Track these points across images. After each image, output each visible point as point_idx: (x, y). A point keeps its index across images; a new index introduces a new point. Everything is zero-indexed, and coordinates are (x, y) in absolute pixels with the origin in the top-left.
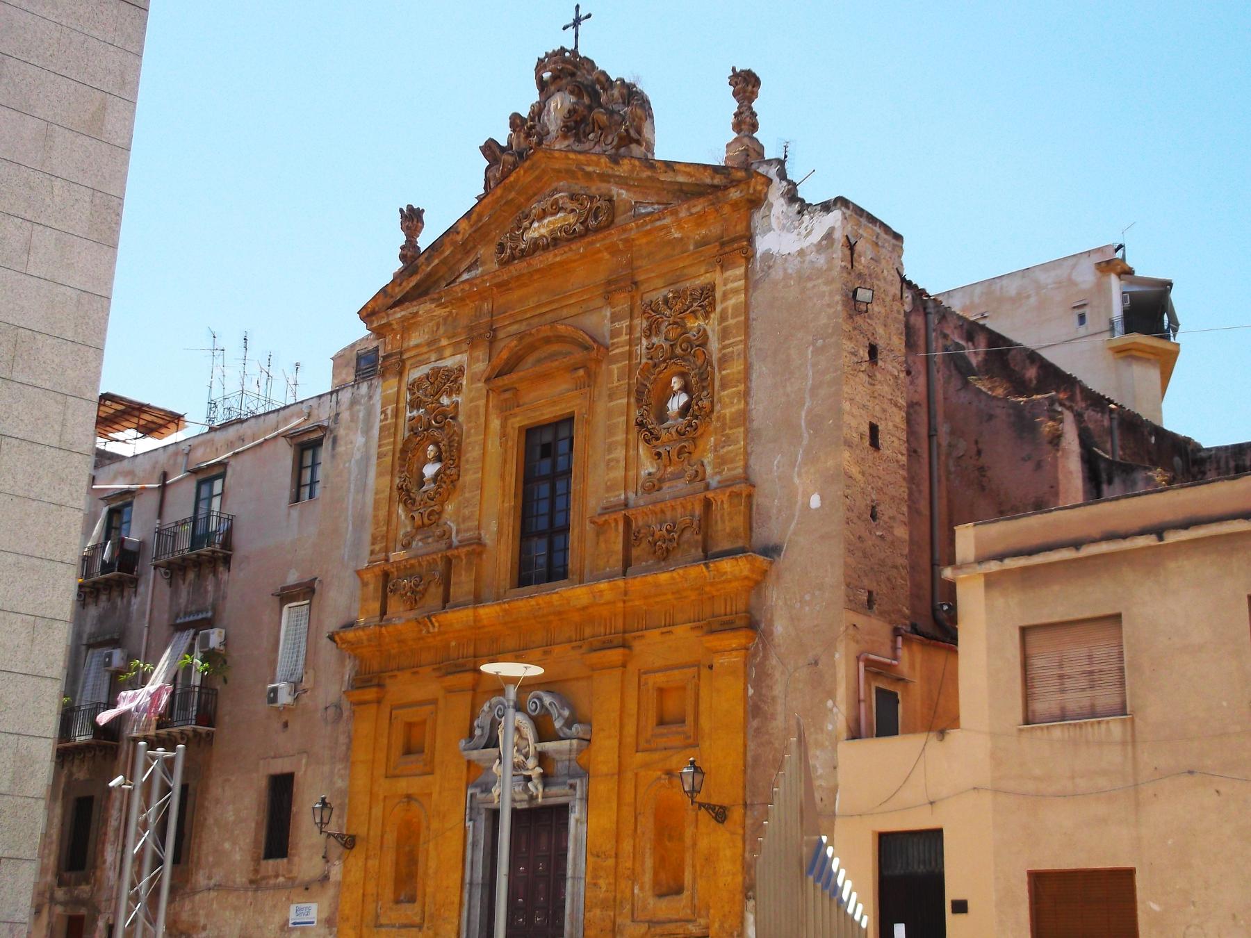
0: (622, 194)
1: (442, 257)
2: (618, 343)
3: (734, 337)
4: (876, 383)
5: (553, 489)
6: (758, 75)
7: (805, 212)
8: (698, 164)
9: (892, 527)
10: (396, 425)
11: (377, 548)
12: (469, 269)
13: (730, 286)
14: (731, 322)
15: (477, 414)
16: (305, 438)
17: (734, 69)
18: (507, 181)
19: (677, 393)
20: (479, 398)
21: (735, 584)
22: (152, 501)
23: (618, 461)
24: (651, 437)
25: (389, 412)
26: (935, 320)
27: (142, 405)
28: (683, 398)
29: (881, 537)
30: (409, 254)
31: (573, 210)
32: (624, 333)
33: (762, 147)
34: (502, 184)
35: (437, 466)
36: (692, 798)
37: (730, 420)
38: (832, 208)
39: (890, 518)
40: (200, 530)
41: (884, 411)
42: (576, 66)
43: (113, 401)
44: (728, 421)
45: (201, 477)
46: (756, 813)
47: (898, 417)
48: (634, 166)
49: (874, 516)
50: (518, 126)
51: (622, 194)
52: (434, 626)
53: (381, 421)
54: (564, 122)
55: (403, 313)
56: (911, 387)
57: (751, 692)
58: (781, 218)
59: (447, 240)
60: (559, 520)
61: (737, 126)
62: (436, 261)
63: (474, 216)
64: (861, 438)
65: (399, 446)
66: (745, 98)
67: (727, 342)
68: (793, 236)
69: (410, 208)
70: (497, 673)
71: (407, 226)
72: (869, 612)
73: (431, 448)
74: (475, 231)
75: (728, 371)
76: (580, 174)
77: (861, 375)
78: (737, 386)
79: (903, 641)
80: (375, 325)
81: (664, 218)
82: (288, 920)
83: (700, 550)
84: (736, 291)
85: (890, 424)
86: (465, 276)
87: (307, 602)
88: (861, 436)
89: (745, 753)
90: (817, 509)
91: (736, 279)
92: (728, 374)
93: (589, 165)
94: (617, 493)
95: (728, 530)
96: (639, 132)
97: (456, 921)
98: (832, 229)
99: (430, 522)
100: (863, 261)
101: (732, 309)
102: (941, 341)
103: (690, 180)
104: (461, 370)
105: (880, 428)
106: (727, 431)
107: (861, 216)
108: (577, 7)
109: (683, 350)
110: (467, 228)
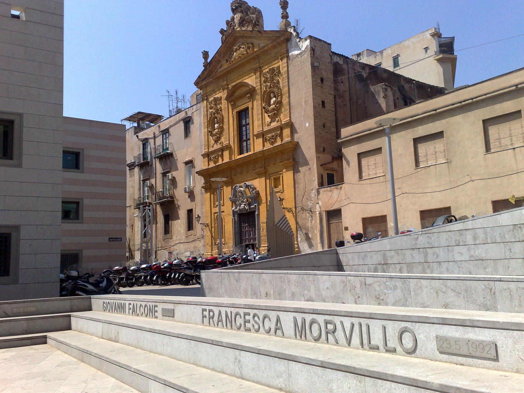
5: (246, 128)
8: (274, 31)
11: (206, 148)
12: (220, 68)
13: (283, 65)
20: (226, 105)
25: (205, 111)
26: (350, 66)
27: (149, 114)
28: (274, 99)
30: (206, 65)
31: (243, 48)
32: (259, 82)
33: (290, 22)
39: (329, 126)
40: (165, 148)
41: (326, 96)
42: (241, 4)
45: (163, 133)
47: (331, 98)
49: (324, 126)
61: (283, 18)
63: (219, 53)
69: (204, 51)
72: (324, 153)
77: (318, 87)
80: (199, 86)
84: (285, 67)
86: (220, 70)
88: (319, 104)
90: (308, 127)
96: (258, 22)
100: (318, 53)
102: (353, 71)
104: (221, 97)
107: (316, 40)
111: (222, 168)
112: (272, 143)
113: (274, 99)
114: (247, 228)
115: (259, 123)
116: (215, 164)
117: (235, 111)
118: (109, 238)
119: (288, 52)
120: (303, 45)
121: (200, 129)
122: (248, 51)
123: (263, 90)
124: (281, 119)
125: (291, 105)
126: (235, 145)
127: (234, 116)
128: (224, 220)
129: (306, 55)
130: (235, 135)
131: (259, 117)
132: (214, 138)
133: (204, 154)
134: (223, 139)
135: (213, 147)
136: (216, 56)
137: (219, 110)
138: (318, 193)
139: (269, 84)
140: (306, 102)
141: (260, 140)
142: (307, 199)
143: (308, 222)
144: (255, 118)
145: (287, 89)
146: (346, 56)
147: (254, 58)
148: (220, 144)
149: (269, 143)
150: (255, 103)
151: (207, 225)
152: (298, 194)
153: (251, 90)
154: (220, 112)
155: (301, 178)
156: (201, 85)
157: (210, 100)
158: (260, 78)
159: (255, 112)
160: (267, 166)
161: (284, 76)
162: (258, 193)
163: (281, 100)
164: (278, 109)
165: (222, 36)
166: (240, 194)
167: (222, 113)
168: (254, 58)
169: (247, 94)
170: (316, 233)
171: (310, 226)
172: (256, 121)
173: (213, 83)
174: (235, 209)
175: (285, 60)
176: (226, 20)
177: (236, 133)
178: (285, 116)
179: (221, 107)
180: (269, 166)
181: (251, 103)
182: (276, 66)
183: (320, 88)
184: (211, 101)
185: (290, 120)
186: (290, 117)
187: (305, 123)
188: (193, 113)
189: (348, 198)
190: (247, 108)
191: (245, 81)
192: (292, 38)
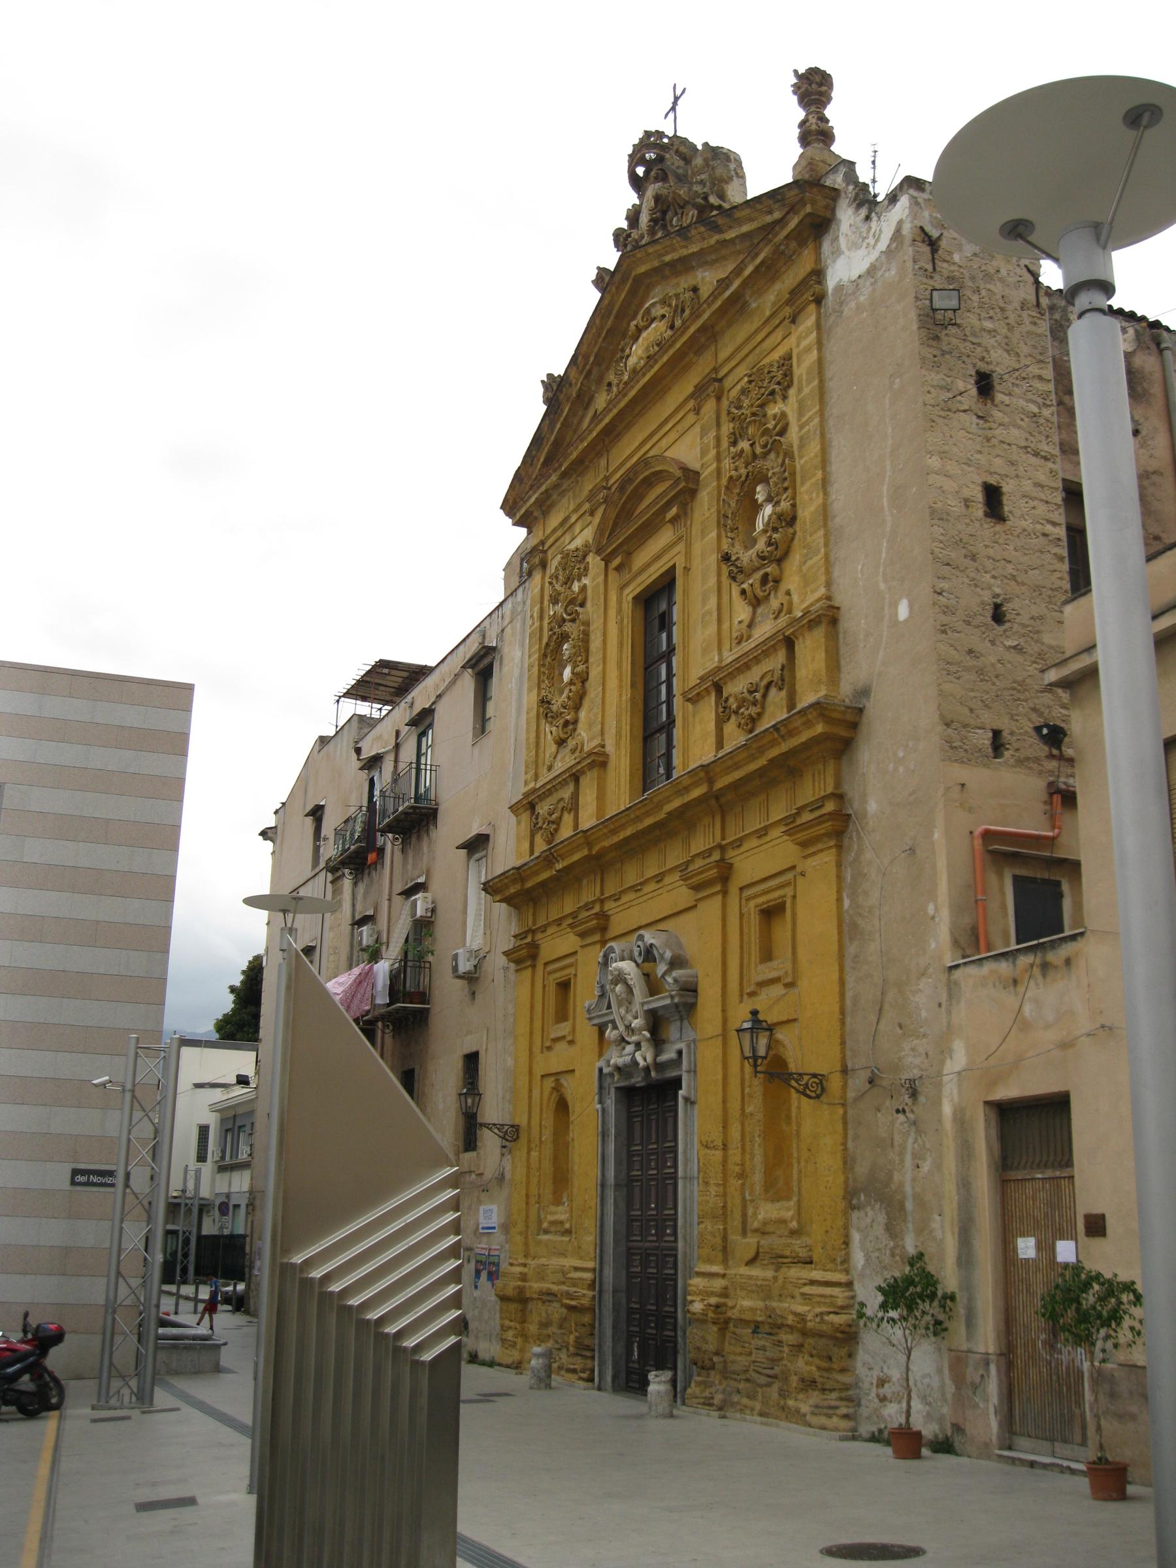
4: (994, 426)
6: (822, 68)
14: (806, 391)
17: (796, 72)
22: (391, 757)
23: (711, 613)
28: (768, 510)
31: (663, 316)
37: (811, 523)
43: (390, 668)
46: (857, 1081)
49: (998, 616)
53: (531, 626)
56: (1142, 451)
57: (846, 903)
61: (805, 138)
62: (558, 426)
64: (967, 506)
68: (862, 252)
84: (808, 350)
88: (967, 503)
89: (842, 995)
98: (900, 223)
105: (1004, 490)
114: (637, 1166)
118: (75, 1172)
120: (884, 229)
138: (952, 989)
143: (902, 1161)
146: (1152, 318)
148: (573, 751)
164: (779, 554)
170: (938, 1234)
171: (908, 1189)
178: (806, 581)
182: (776, 355)
183: (970, 420)
185: (829, 598)
186: (829, 584)
187: (894, 605)
189: (1103, 1026)
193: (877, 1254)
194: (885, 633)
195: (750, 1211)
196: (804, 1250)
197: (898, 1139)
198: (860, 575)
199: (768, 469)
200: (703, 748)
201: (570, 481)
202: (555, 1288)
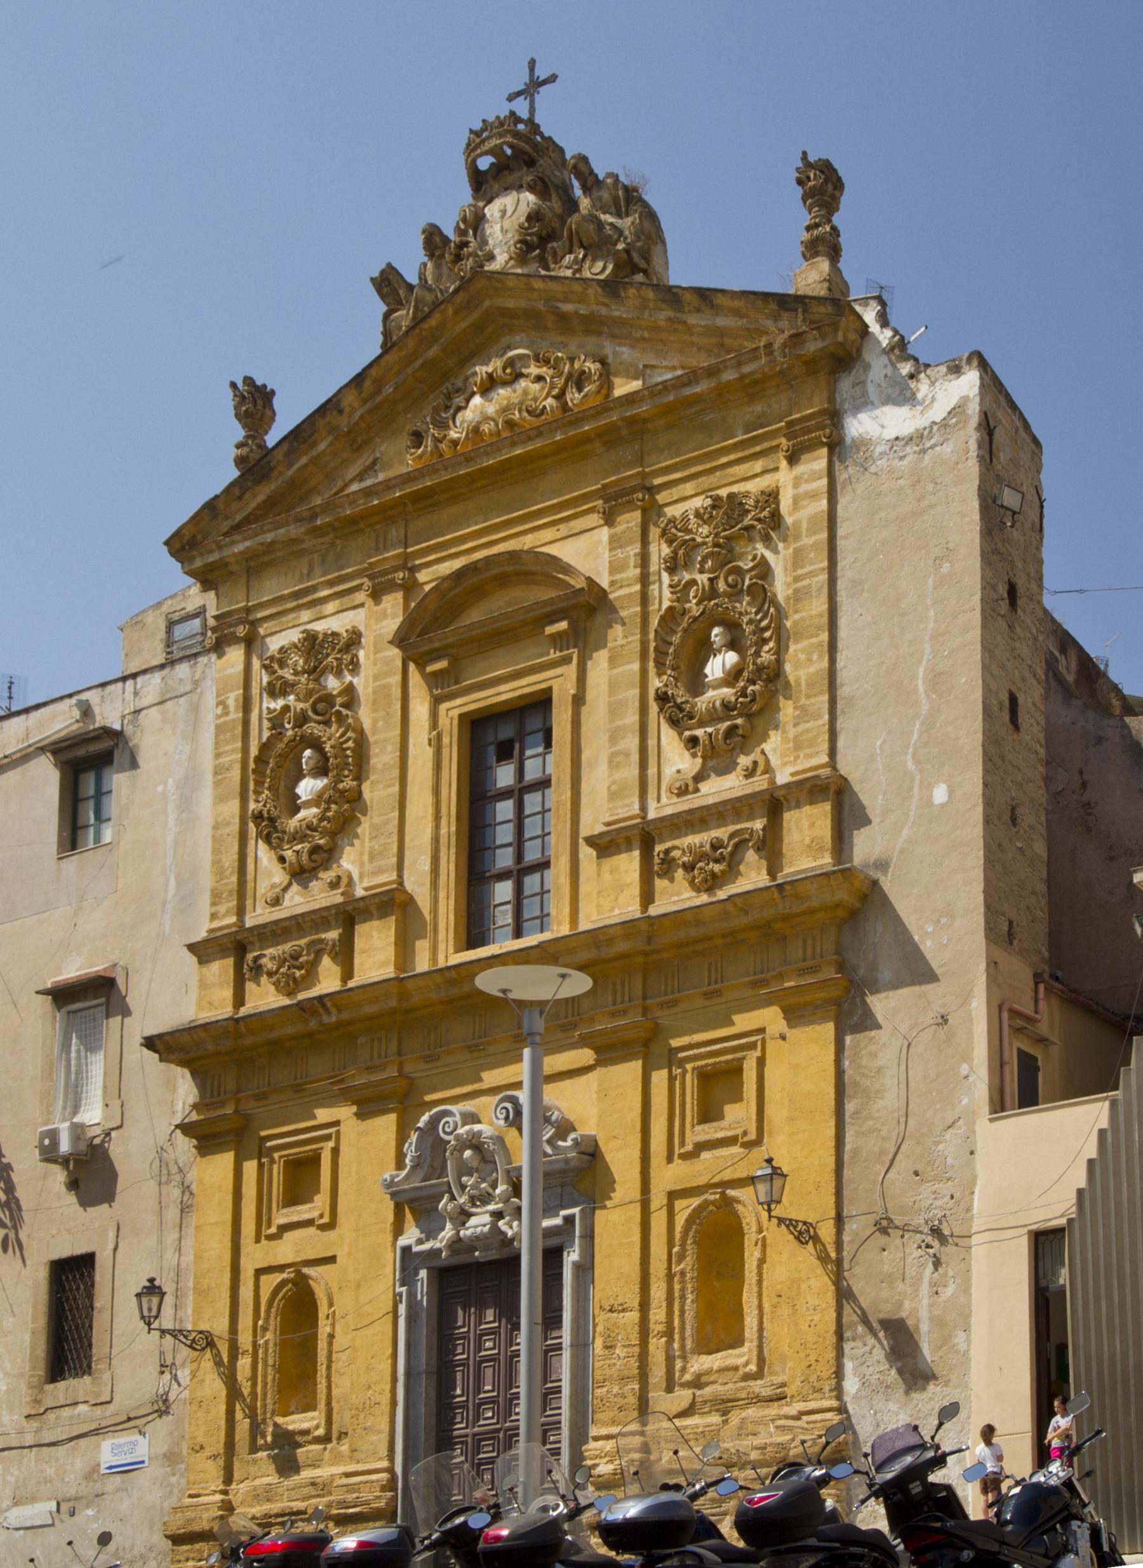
0: (623, 353)
1: (314, 453)
2: (622, 580)
3: (812, 564)
5: (520, 807)
7: (922, 376)
8: (754, 293)
9: (1032, 839)
10: (246, 723)
12: (361, 477)
15: (388, 696)
16: (81, 752)
18: (425, 326)
19: (720, 652)
20: (388, 674)
21: (821, 915)
24: (678, 718)
25: (231, 703)
28: (731, 658)
29: (1020, 849)
31: (539, 379)
32: (632, 563)
34: (417, 331)
35: (320, 783)
36: (769, 1210)
38: (965, 368)
44: (803, 686)
48: (645, 299)
49: (1014, 820)
50: (437, 247)
51: (623, 353)
52: (328, 1013)
54: (520, 234)
55: (247, 544)
58: (884, 385)
59: (320, 423)
60: (532, 854)
62: (304, 460)
63: (368, 384)
65: (254, 751)
66: (822, 205)
67: (800, 572)
69: (249, 381)
70: (504, 991)
71: (246, 411)
73: (308, 753)
74: (370, 412)
75: (804, 614)
76: (550, 321)
78: (817, 635)
79: (1046, 988)
80: (198, 563)
81: (697, 383)
82: (99, 1465)
83: (764, 872)
84: (813, 496)
85: (1030, 700)
86: (355, 487)
87: (103, 1000)
90: (943, 805)
91: (813, 477)
92: (803, 619)
93: (567, 300)
94: (627, 801)
95: (807, 841)
96: (647, 260)
97: (385, 1427)
99: (313, 865)
101: (809, 523)
103: (739, 323)
106: (803, 701)
108: (532, 64)
109: (729, 586)
110: (356, 404)
111: (344, 1016)
112: (712, 883)
113: (731, 658)
114: (489, 1344)
115: (618, 775)
116: (290, 994)
117: (453, 710)
119: (834, 417)
121: (186, 804)
122: (573, 397)
123: (654, 607)
124: (767, 761)
125: (843, 692)
126: (442, 894)
127: (446, 740)
128: (331, 1305)
129: (948, 448)
130: (443, 840)
131: (621, 746)
132: (289, 854)
133: (205, 942)
134: (349, 862)
135: (276, 902)
136: (349, 399)
137: (339, 700)
139: (703, 579)
140: (936, 680)
141: (629, 864)
142: (916, 1174)
144: (595, 749)
145: (820, 605)
147: (610, 438)
148: (334, 885)
149: (692, 883)
150: (599, 666)
151: (206, 1342)
152: (856, 1152)
153: (582, 599)
154: (345, 712)
155: (879, 1070)
156: (212, 558)
157: (274, 644)
158: (645, 542)
159: (595, 716)
160: (661, 1005)
161: (807, 541)
162: (591, 1153)
163: (779, 663)
165: (384, 308)
166: (468, 1153)
167: (357, 720)
168: (610, 438)
169: (553, 618)
171: (924, 1313)
172: (602, 769)
173: (301, 553)
174: (420, 1242)
175: (817, 462)
176: (422, 225)
177: (449, 827)
179: (350, 690)
180: (673, 1003)
181: (571, 670)
182: (753, 487)
184: (282, 650)
186: (832, 752)
188: (137, 712)
190: (542, 702)
191: (552, 550)
192: (869, 356)
193: (877, 1376)
194: (912, 813)
195: (679, 1364)
196: (768, 1389)
197: (911, 1272)
198: (878, 751)
199: (741, 614)
200: (616, 899)
201: (320, 540)
202: (298, 1505)
